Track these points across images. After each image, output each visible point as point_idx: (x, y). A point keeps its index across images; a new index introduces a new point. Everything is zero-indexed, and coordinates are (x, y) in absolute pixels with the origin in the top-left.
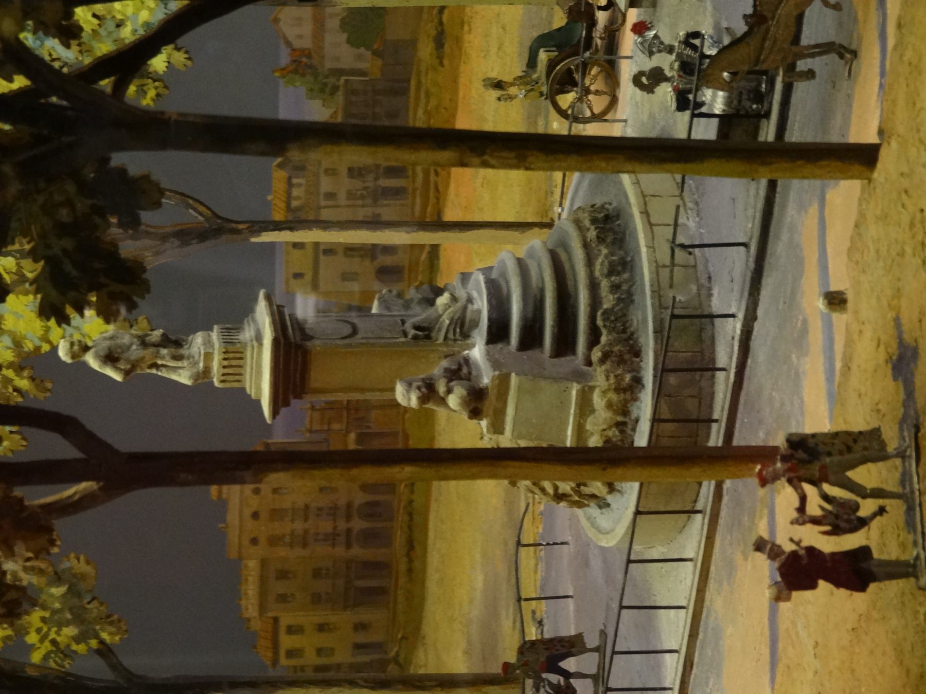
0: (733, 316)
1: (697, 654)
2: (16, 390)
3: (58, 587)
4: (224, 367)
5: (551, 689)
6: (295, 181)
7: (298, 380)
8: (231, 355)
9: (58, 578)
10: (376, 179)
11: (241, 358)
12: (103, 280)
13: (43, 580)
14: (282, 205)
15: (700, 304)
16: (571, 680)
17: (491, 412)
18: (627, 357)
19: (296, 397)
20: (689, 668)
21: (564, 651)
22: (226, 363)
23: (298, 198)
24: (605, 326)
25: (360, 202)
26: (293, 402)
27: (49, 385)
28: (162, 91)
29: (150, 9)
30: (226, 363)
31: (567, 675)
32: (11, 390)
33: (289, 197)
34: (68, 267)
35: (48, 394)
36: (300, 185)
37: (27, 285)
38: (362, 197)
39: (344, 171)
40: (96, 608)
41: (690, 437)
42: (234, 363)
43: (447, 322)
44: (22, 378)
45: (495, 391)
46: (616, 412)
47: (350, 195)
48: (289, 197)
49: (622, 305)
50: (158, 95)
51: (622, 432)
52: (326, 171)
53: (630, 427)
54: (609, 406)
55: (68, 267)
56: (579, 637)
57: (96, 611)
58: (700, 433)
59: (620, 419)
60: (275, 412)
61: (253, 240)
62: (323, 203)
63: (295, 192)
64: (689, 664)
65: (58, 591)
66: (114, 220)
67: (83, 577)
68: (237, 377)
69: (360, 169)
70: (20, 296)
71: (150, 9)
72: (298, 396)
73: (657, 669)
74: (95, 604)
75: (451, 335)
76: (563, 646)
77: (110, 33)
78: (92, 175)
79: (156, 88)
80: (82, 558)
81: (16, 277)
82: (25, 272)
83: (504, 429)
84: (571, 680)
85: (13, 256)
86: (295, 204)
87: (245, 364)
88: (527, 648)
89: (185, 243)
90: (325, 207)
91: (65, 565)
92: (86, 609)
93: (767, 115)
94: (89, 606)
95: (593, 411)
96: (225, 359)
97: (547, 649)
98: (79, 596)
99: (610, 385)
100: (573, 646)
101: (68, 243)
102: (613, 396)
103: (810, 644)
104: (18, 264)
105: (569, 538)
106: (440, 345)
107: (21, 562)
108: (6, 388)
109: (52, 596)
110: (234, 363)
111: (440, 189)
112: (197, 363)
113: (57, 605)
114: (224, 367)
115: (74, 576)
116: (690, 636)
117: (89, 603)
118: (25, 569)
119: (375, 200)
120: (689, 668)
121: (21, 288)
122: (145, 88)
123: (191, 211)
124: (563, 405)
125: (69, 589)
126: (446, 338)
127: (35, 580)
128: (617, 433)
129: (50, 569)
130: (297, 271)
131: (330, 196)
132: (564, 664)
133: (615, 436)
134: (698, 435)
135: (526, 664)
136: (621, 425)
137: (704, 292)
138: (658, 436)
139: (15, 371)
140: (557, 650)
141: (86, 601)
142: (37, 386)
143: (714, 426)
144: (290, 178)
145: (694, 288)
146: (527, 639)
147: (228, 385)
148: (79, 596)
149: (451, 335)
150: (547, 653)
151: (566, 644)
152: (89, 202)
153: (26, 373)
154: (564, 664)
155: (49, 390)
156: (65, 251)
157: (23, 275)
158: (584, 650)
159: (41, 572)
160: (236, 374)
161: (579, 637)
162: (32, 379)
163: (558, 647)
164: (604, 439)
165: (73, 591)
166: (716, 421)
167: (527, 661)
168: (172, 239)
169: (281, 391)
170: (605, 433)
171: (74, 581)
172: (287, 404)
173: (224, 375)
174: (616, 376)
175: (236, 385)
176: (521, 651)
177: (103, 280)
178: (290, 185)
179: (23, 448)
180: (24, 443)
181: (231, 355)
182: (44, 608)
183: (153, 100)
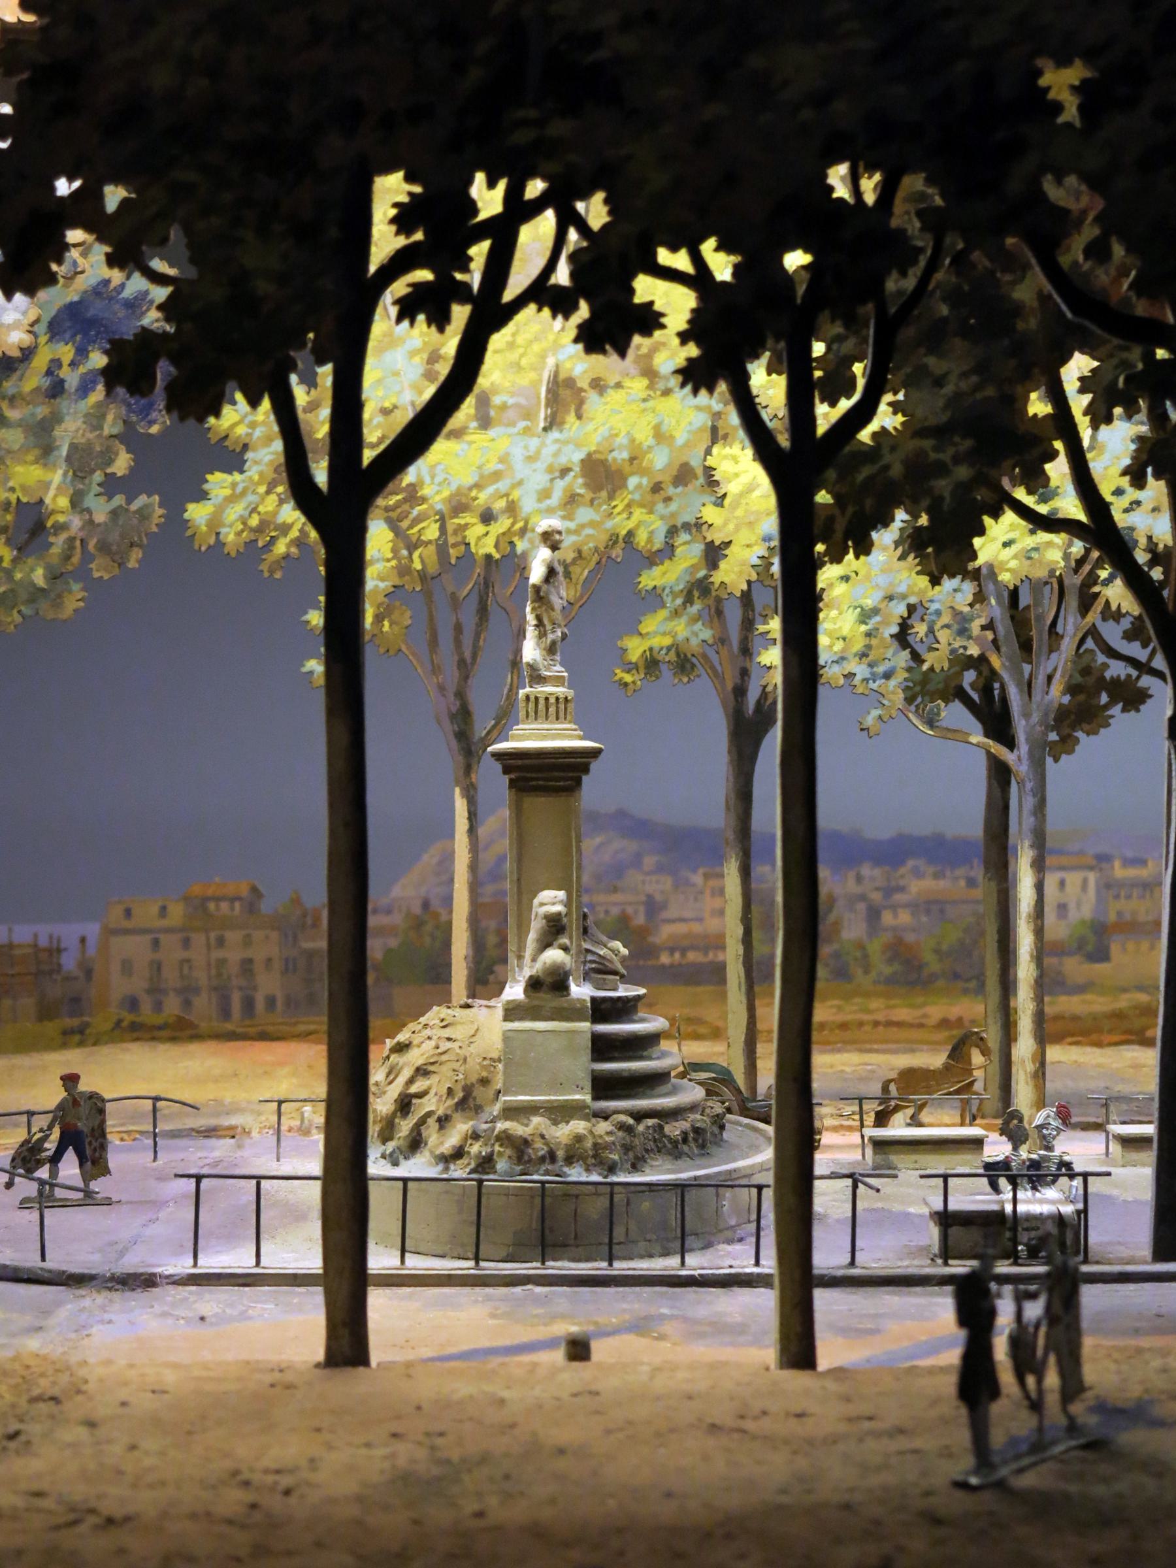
0: (757, 1263)
1: (267, 1288)
2: (273, 540)
3: (45, 577)
4: (547, 699)
5: (38, 1140)
6: (237, 905)
7: (534, 783)
8: (562, 706)
9: (54, 577)
10: (240, 988)
11: (557, 718)
12: (850, 510)
13: (55, 560)
14: (210, 892)
15: (721, 1231)
16: (47, 1166)
17: (536, 1003)
18: (631, 1154)
19: (511, 781)
20: (241, 1281)
21: (88, 1152)
22: (552, 700)
23: (218, 908)
24: (648, 1127)
25: (213, 972)
26: (506, 779)
27: (278, 575)
28: (631, 687)
29: (831, 647)
30: (552, 700)
31: (56, 1159)
32: (273, 534)
33: (218, 899)
34: (865, 472)
35: (266, 574)
36: (232, 909)
37: (405, 552)
38: (219, 975)
39: (249, 954)
40: (13, 621)
41: (576, 1237)
42: (552, 710)
43: (601, 953)
44: (288, 546)
45: (565, 1005)
46: (569, 1148)
47: (222, 962)
48: (218, 899)
49: (669, 1146)
50: (626, 684)
51: (542, 1159)
52: (248, 935)
53: (550, 1167)
54: (579, 1138)
55: (865, 472)
56: (106, 1171)
57: (9, 620)
58: (580, 1249)
59: (560, 1154)
60: (498, 756)
61: (457, 790)
62: (213, 935)
63: (224, 906)
64: (248, 1280)
65: (39, 576)
66: (924, 520)
67: (57, 603)
68: (532, 714)
69: (251, 971)
70: (391, 544)
71: (831, 647)
72: (513, 784)
73: (229, 1238)
74: (18, 619)
75: (590, 957)
76: (95, 1150)
77: (696, 635)
78: (979, 497)
79: (634, 682)
80: (82, 604)
81: (414, 539)
82: (420, 550)
83: (512, 1021)
84: (47, 1166)
85: (439, 538)
86: (212, 906)
87: (552, 723)
88: (97, 1104)
89: (453, 717)
90: (208, 939)
91: (76, 587)
92: (13, 608)
93: (1016, 1264)
94: (15, 612)
95: (555, 1123)
96: (557, 699)
97: (93, 1130)
98: (32, 600)
99: (601, 1137)
100: (94, 1163)
101: (897, 470)
102: (589, 1144)
103: (506, 1394)
104: (430, 542)
105: (160, 1162)
106: (579, 946)
107: (81, 535)
108: (275, 529)
109: (32, 570)
110: (552, 710)
111: (311, 1037)
112: (548, 669)
113: (18, 576)
114: (547, 699)
115: (60, 596)
116: (295, 1276)
117: (19, 612)
118: (71, 540)
119: (215, 989)
120: (241, 1281)
121: (402, 545)
122: (634, 671)
123: (493, 722)
124: (558, 1085)
125: (42, 590)
126: (588, 951)
127: (56, 550)
128: (541, 1153)
129: (70, 568)
130: (133, 912)
131: (221, 942)
132: (70, 1156)
133: (536, 1150)
134: (577, 1246)
135: (75, 1103)
136: (552, 1156)
137: (729, 1234)
138: (577, 1196)
139: (298, 539)
140: (90, 1143)
141: (23, 608)
142: (278, 562)
143: (605, 1264)
144: (239, 899)
145: (733, 1222)
146: (108, 1105)
147: (522, 704)
148: (32, 600)
149: (590, 957)
150: (86, 1130)
151: (97, 1154)
152: (947, 494)
153: (294, 550)
154: (70, 1156)
155: (271, 575)
156: (887, 468)
157: (416, 547)
158: (87, 1177)
159: (67, 557)
160: (536, 712)
161: (106, 1171)
162: (286, 557)
163: (95, 1144)
164: (529, 1138)
165: (37, 594)
166: (611, 1265)
167: (79, 1105)
168: (458, 703)
169: (527, 762)
170: (538, 1139)
171: (53, 595)
172: (506, 770)
173: (537, 698)
174: (613, 1143)
175: (522, 714)
176: (93, 1097)
177: (850, 510)
178: (233, 900)
179: (196, 547)
180: (203, 549)
181: (562, 706)
182: (15, 561)
183: (621, 680)
